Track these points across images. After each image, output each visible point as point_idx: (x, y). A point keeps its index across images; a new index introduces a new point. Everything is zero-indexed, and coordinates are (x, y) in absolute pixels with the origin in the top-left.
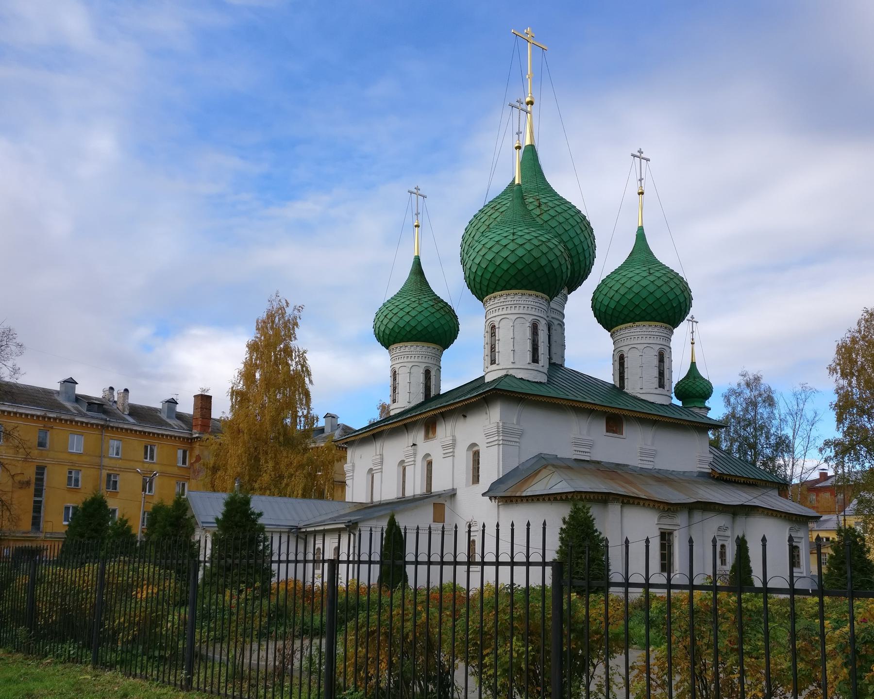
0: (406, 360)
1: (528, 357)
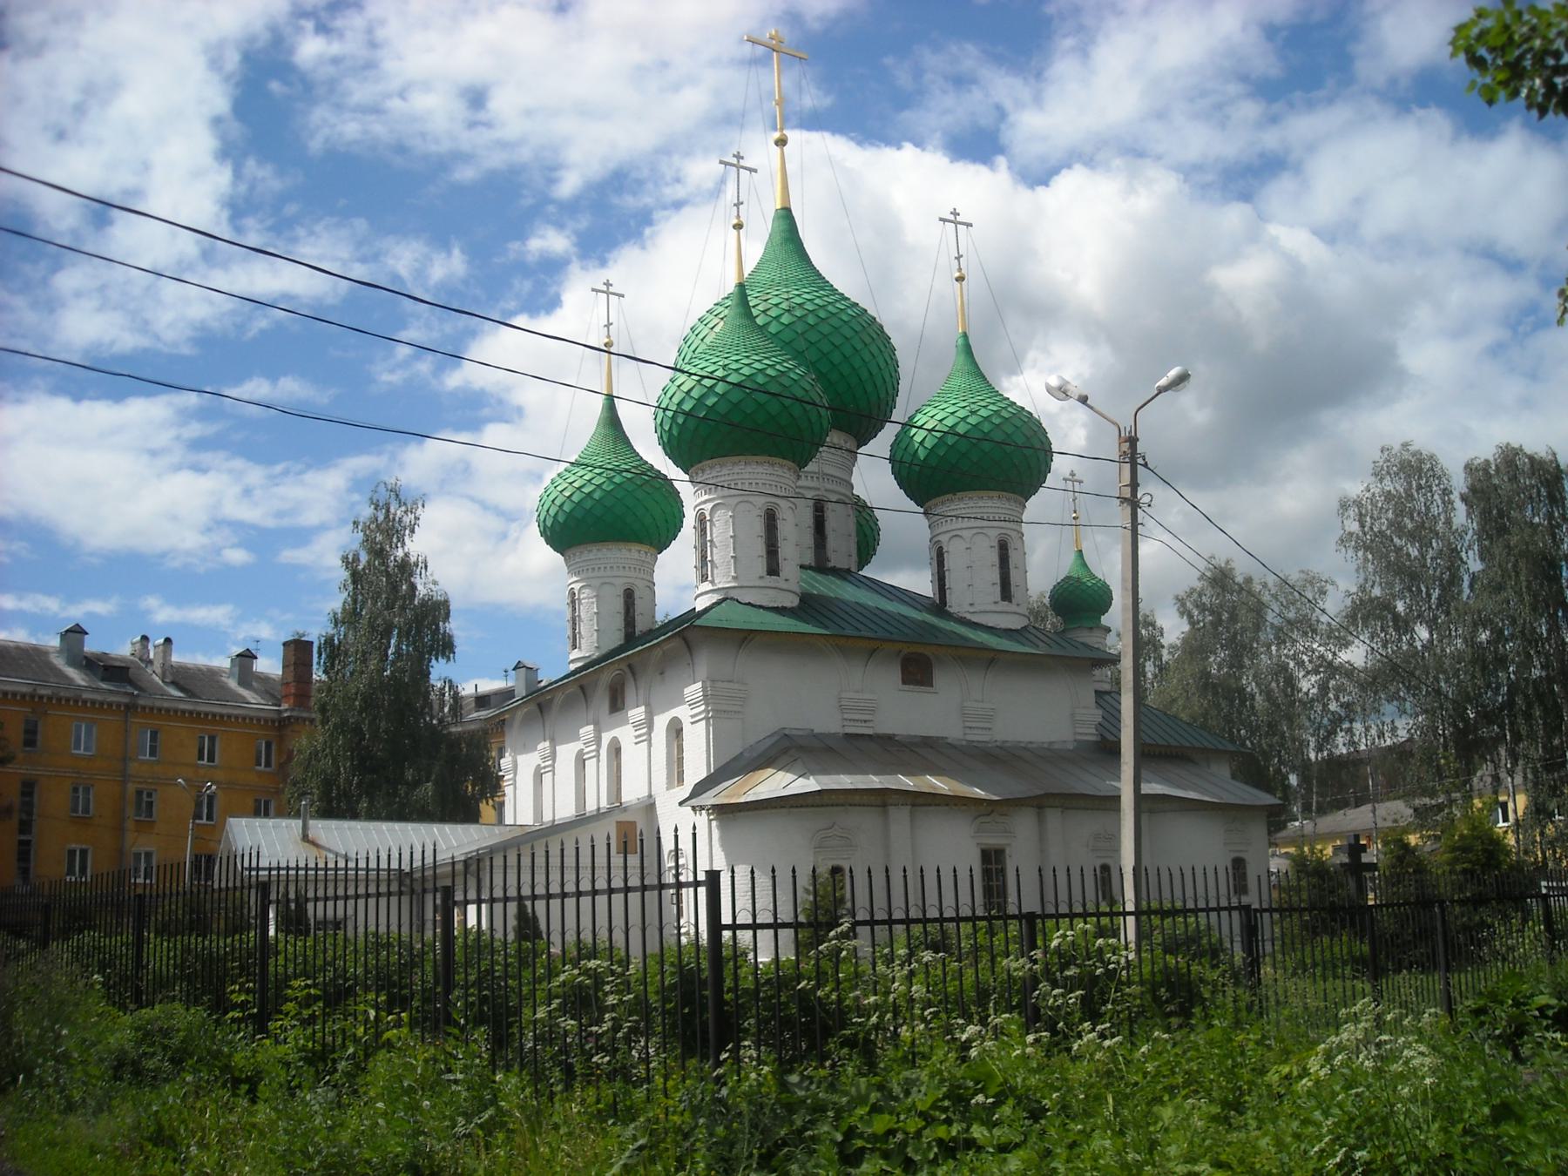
0: (609, 573)
1: (761, 566)
